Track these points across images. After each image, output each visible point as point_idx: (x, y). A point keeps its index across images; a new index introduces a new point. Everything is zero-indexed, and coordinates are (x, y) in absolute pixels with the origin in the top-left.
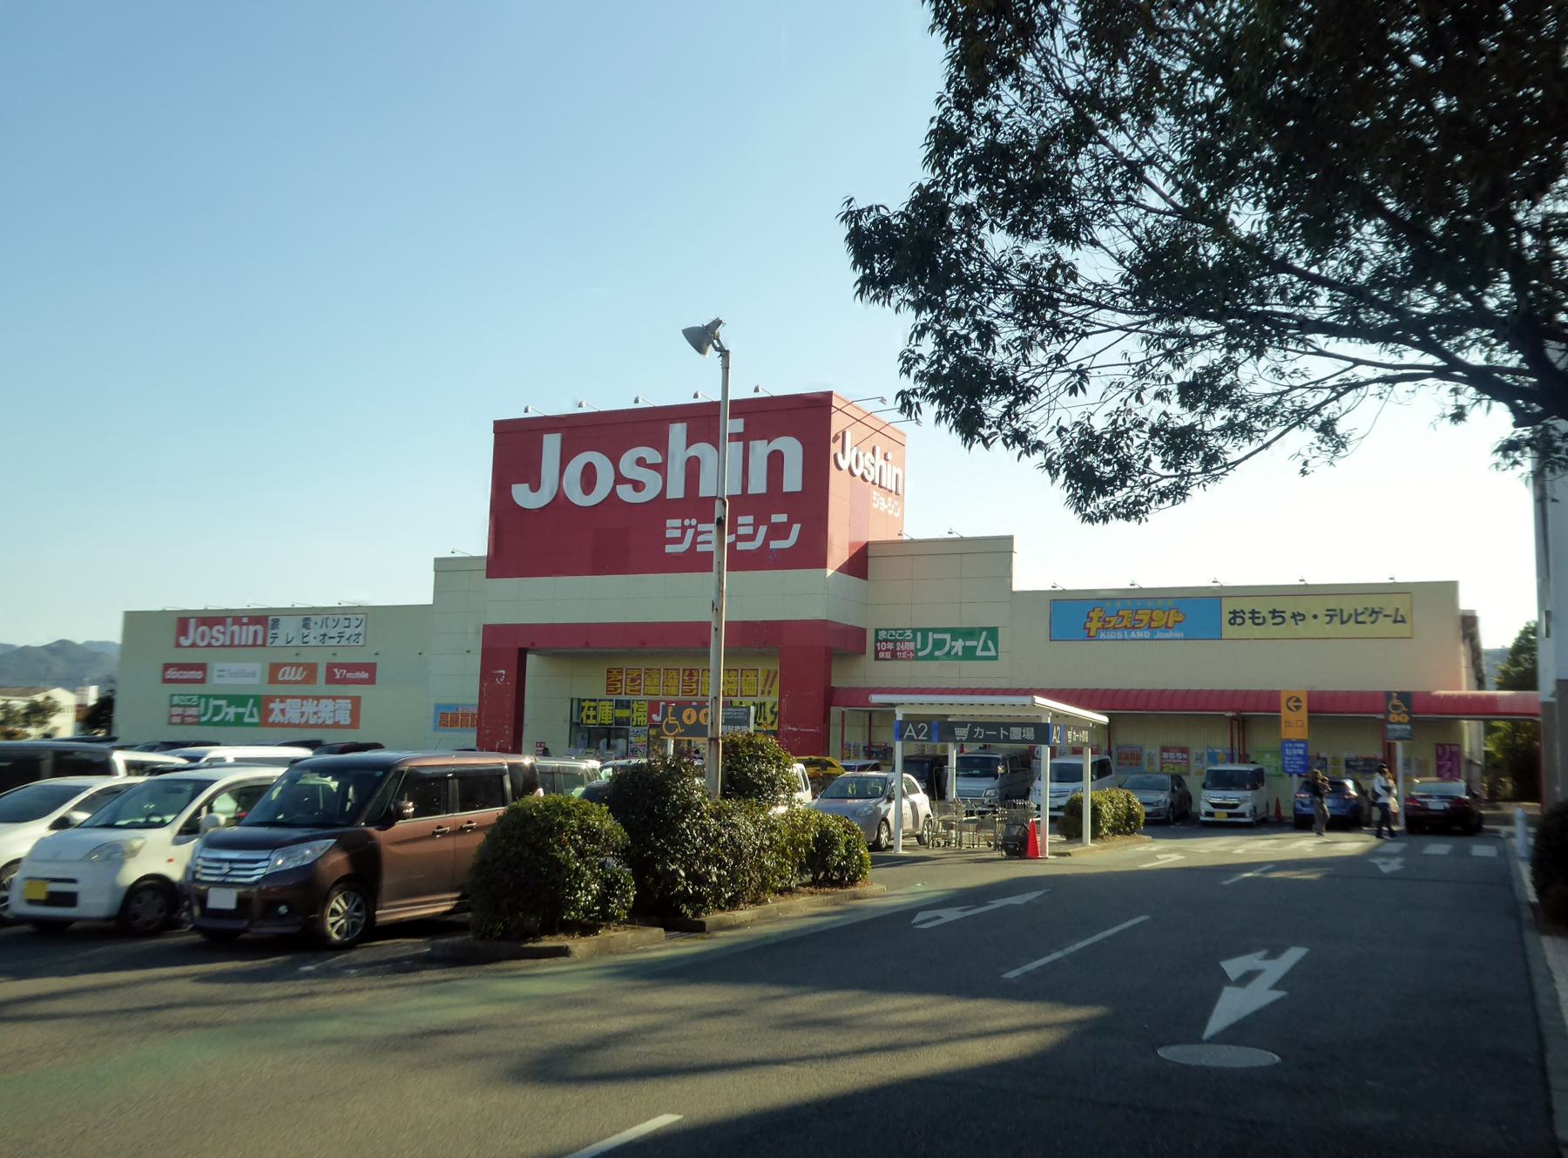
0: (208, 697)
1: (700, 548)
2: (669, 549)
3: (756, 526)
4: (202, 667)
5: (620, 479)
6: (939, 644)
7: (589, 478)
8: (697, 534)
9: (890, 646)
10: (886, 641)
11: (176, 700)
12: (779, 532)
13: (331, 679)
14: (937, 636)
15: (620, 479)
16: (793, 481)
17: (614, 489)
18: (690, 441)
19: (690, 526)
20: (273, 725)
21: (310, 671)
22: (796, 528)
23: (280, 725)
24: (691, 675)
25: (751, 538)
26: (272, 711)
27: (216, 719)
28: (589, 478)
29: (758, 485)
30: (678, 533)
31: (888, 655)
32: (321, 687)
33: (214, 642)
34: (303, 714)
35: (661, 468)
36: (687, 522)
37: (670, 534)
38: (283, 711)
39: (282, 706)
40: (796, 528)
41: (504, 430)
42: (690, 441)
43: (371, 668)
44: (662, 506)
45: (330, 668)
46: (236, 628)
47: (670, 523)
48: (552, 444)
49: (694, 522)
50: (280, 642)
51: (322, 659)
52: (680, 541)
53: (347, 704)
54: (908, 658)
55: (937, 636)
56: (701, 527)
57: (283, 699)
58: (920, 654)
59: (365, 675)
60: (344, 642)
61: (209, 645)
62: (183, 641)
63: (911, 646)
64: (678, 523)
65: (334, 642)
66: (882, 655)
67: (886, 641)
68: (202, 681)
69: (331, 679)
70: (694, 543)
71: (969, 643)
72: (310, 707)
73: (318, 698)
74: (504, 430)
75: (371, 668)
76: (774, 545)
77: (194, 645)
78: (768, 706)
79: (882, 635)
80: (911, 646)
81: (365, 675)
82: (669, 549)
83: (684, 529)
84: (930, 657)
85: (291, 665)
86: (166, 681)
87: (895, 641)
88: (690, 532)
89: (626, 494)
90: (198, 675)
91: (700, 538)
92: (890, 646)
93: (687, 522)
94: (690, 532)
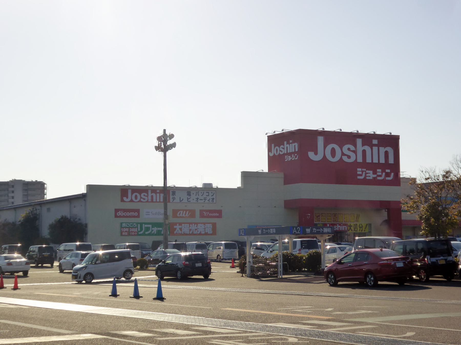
0: (141, 224)
1: (368, 178)
2: (359, 177)
3: (382, 172)
4: (138, 211)
5: (343, 154)
6: (147, 229)
7: (333, 152)
8: (366, 173)
9: (127, 230)
10: (126, 227)
11: (124, 225)
12: (388, 175)
13: (202, 216)
14: (146, 226)
15: (343, 154)
16: (391, 161)
17: (341, 157)
18: (363, 145)
19: (364, 171)
20: (177, 234)
21: (192, 214)
22: (392, 174)
23: (181, 234)
24: (335, 216)
25: (380, 176)
26: (176, 229)
27: (147, 233)
28: (333, 152)
29: (382, 161)
30: (360, 173)
31: (126, 234)
32: (198, 219)
33: (142, 200)
34: (190, 230)
35: (355, 152)
36: (363, 170)
37: (358, 173)
38: (181, 229)
39: (180, 227)
40: (392, 174)
41: (396, 139)
42: (363, 145)
43: (220, 212)
44: (356, 164)
45: (201, 211)
46: (154, 194)
47: (358, 169)
48: (321, 140)
49: (365, 170)
50: (177, 200)
51: (197, 208)
52: (361, 175)
53: (210, 226)
54: (135, 235)
55: (146, 226)
56: (367, 171)
57: (180, 224)
58: (139, 233)
59: (218, 215)
60: (207, 201)
61: (140, 201)
62: (125, 199)
63: (135, 230)
64: (360, 169)
65: (203, 201)
66: (124, 233)
67: (126, 227)
68: (138, 216)
69: (202, 216)
70: (366, 176)
71: (159, 229)
72: (193, 227)
73: (197, 224)
74: (396, 139)
75: (220, 212)
76: (388, 178)
77: (132, 201)
78: (358, 225)
79: (124, 225)
80: (135, 230)
81: (218, 215)
82: (359, 177)
83: (362, 171)
84: (144, 234)
85: (183, 210)
86: (116, 216)
87: (129, 228)
88: (364, 173)
89: (345, 159)
90: (136, 214)
91: (367, 175)
92: (127, 230)
93: (363, 170)
94: (364, 173)
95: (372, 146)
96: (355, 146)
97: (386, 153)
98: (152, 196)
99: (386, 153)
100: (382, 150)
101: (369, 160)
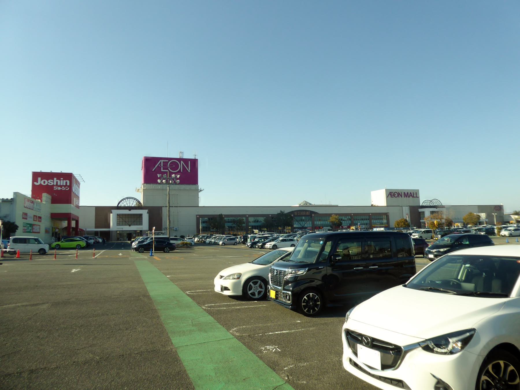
7: (44, 182)
28: (44, 182)
29: (64, 184)
44: (53, 185)
89: (49, 184)
95: (60, 180)
96: (53, 180)
97: (66, 183)
98: (57, 182)
99: (66, 183)
100: (65, 181)
101: (59, 184)
